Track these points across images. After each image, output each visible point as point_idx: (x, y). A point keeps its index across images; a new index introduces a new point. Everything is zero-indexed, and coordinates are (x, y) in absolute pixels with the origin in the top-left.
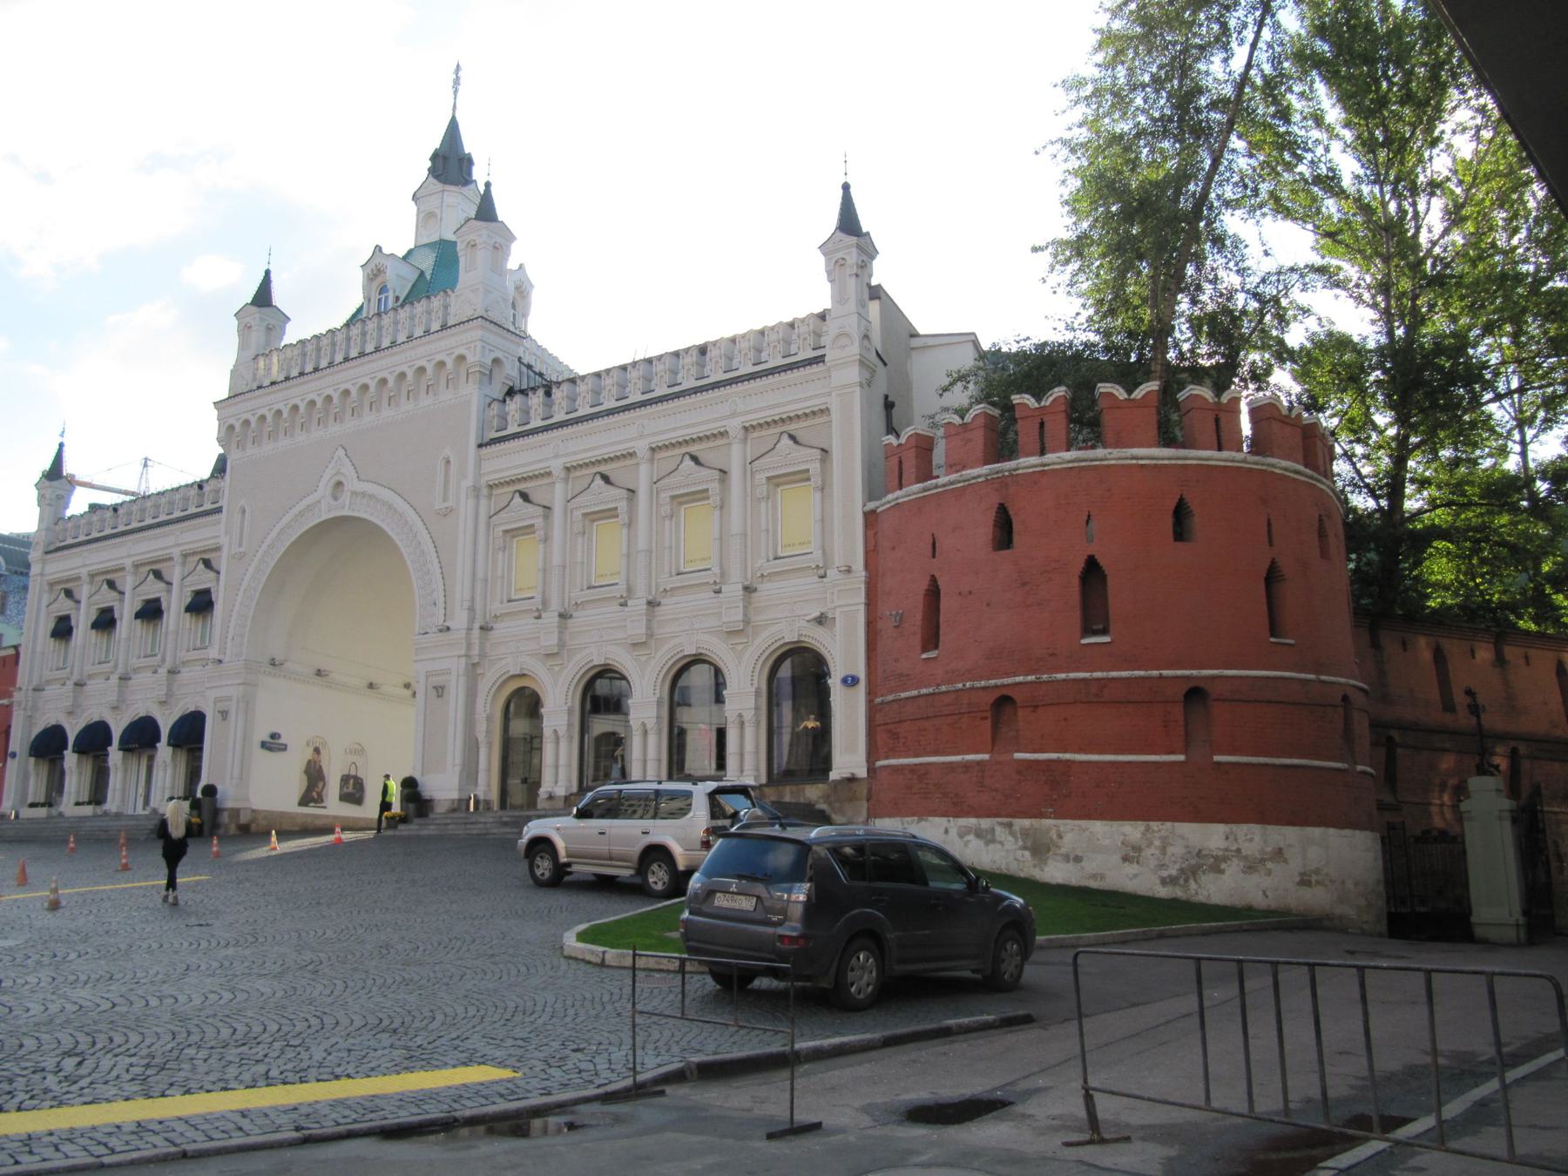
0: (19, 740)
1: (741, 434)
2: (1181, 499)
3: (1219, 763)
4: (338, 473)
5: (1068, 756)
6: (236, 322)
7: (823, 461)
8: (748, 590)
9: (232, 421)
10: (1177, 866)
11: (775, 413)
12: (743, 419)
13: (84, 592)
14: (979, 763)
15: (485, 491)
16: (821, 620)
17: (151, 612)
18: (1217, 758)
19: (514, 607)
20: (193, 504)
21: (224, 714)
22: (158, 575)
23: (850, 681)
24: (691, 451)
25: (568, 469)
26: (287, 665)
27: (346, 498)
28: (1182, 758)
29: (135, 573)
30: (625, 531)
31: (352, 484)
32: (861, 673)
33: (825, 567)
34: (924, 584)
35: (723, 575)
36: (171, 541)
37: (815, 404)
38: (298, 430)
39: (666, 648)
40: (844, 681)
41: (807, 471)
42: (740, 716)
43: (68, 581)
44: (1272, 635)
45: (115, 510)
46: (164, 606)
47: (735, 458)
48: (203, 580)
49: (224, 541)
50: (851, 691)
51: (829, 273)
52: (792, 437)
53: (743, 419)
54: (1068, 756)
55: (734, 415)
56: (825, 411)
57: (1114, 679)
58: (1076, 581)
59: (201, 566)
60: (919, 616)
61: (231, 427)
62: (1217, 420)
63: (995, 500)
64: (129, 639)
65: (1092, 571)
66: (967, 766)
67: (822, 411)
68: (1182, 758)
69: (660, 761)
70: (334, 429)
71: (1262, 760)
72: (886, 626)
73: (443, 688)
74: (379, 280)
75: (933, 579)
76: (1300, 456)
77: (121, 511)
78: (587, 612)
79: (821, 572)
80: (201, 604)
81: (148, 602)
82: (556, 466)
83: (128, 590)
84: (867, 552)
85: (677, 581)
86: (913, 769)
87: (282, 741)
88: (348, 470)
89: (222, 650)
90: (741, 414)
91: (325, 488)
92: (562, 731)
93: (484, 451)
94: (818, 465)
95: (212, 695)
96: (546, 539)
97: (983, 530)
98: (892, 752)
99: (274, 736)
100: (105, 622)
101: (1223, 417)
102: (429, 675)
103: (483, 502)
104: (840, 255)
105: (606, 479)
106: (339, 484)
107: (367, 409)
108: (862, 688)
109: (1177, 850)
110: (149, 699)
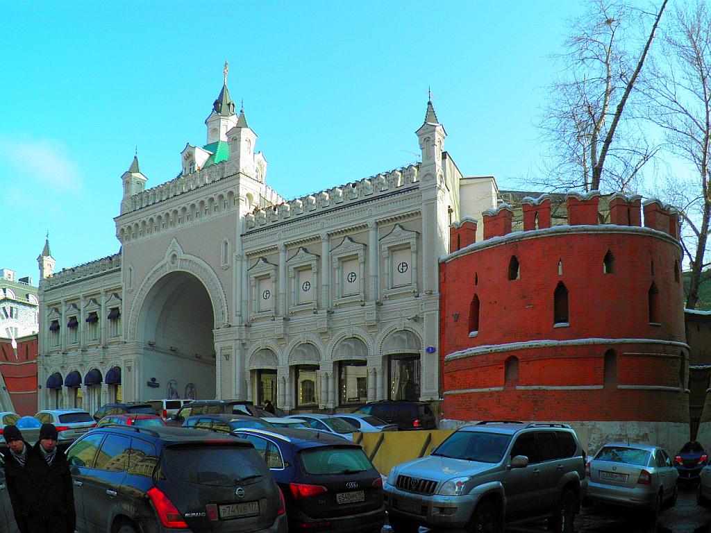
0: (43, 379)
1: (374, 226)
2: (609, 251)
3: (620, 389)
4: (173, 250)
5: (544, 387)
6: (122, 181)
7: (417, 238)
8: (379, 304)
9: (122, 227)
10: (595, 445)
11: (393, 215)
12: (376, 218)
13: (82, 305)
14: (497, 392)
15: (245, 257)
16: (416, 319)
17: (93, 319)
18: (620, 387)
19: (395, 292)
20: (110, 264)
21: (129, 369)
22: (95, 301)
23: (431, 351)
24: (303, 245)
25: (85, 297)
26: (156, 345)
27: (178, 262)
28: (602, 387)
29: (106, 296)
30: (315, 276)
31: (181, 255)
32: (436, 345)
33: (418, 292)
34: (472, 298)
35: (365, 297)
36: (99, 285)
37: (361, 222)
38: (177, 222)
39: (336, 335)
40: (428, 350)
41: (269, 274)
42: (374, 369)
43: (56, 304)
44: (650, 322)
45: (73, 270)
46: (98, 316)
47: (324, 249)
48: (114, 303)
49: (122, 284)
50: (431, 355)
51: (421, 145)
52: (401, 227)
53: (376, 218)
54: (544, 387)
55: (371, 216)
56: (419, 213)
57: (656, 339)
58: (552, 295)
59: (113, 296)
60: (468, 315)
61: (123, 230)
62: (629, 211)
63: (510, 254)
64: (84, 332)
65: (561, 291)
66: (491, 394)
67: (417, 213)
68: (602, 387)
69: (334, 392)
70: (171, 229)
71: (641, 387)
72: (450, 320)
73: (228, 355)
74: (190, 159)
75: (476, 296)
76: (668, 230)
77: (114, 260)
78: (298, 317)
79: (416, 294)
80: (115, 315)
81: (91, 314)
82: (280, 244)
83: (103, 304)
84: (440, 284)
85: (299, 308)
86: (463, 396)
87: (156, 382)
88: (178, 248)
89: (126, 338)
90: (374, 216)
91: (168, 258)
92: (287, 377)
93: (244, 238)
94: (315, 262)
95: (123, 359)
96: (276, 281)
97: (504, 270)
98: (452, 387)
99: (154, 380)
100: (93, 319)
101: (633, 210)
102: (125, 362)
103: (245, 263)
104: (427, 136)
105: (305, 250)
106: (175, 256)
107: (177, 222)
108: (436, 355)
109: (595, 436)
110: (93, 361)
